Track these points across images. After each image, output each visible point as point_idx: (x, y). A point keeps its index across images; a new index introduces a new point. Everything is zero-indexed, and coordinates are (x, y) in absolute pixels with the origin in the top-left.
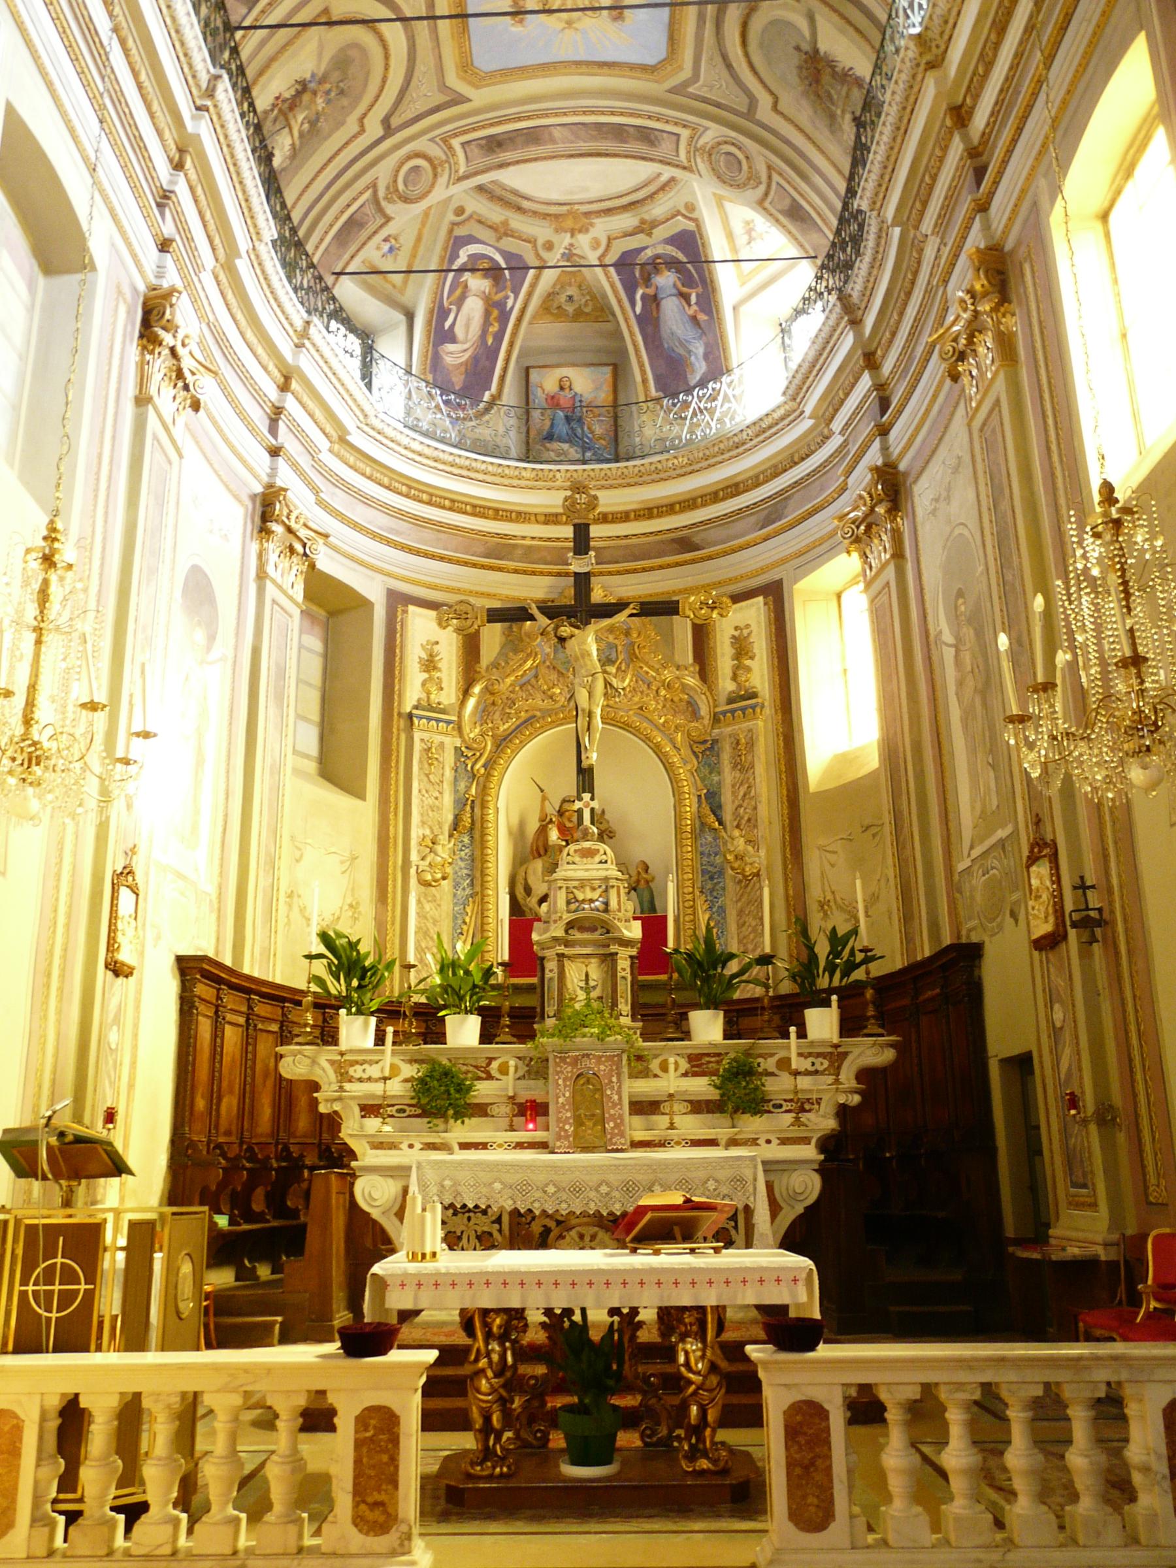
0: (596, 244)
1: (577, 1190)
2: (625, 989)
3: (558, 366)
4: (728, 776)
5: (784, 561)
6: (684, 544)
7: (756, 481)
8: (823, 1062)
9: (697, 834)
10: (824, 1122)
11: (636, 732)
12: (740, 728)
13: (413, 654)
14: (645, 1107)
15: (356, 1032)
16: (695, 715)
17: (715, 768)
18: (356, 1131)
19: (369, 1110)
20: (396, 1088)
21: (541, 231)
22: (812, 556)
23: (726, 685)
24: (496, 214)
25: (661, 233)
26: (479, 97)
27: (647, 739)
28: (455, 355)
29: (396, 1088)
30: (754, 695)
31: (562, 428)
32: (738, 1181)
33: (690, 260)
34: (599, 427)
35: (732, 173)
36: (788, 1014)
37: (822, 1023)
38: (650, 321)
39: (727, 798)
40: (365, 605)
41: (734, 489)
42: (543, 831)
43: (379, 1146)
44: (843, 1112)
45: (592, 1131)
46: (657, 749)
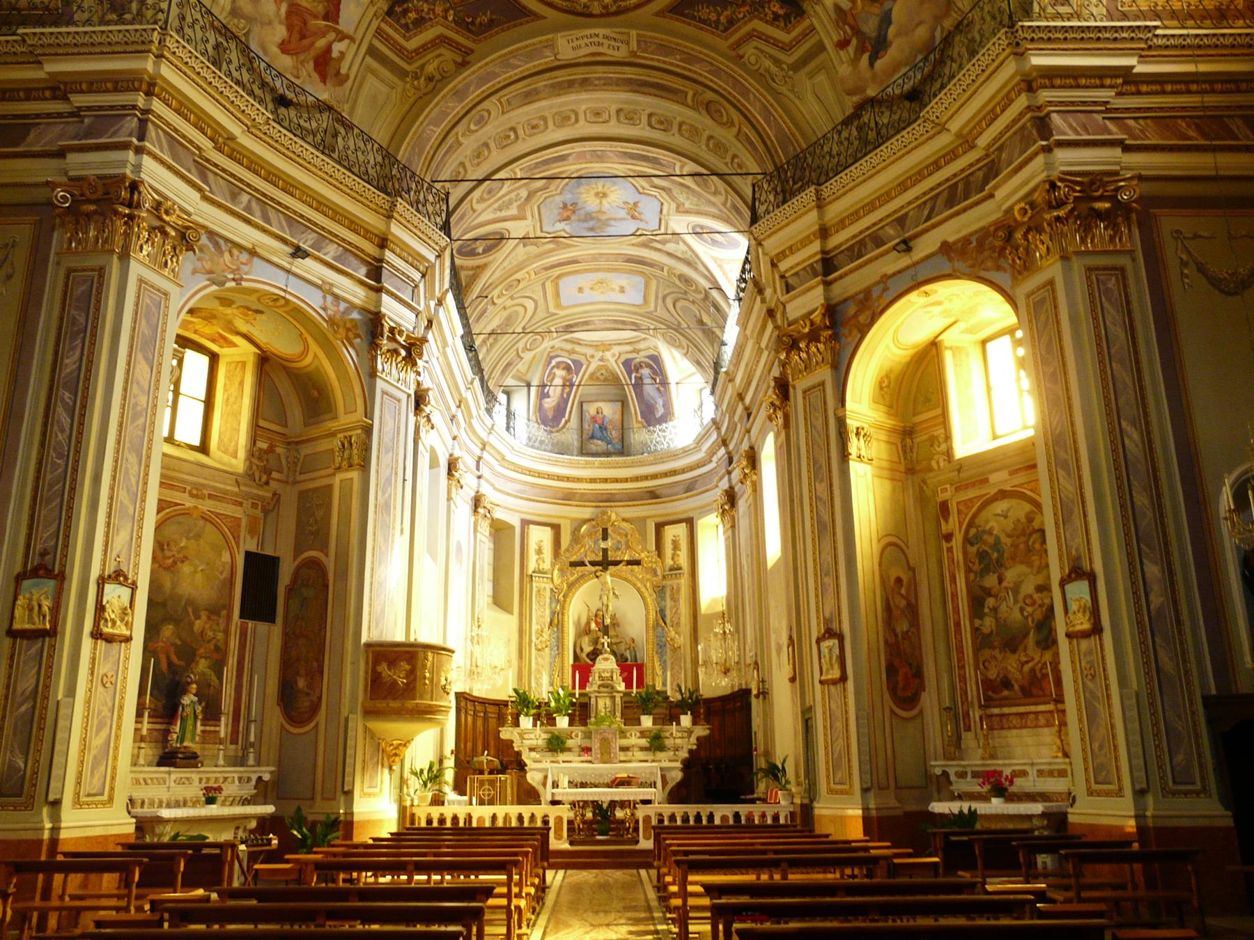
0: (614, 355)
1: (601, 776)
2: (619, 708)
3: (596, 401)
4: (669, 603)
5: (694, 509)
6: (653, 495)
7: (683, 471)
8: (686, 733)
9: (654, 628)
10: (684, 754)
11: (629, 582)
12: (674, 582)
13: (532, 547)
14: (624, 749)
15: (526, 722)
16: (655, 574)
17: (663, 599)
18: (526, 757)
19: (532, 749)
20: (540, 742)
21: (589, 351)
22: (705, 510)
23: (669, 562)
24: (569, 346)
25: (642, 354)
26: (562, 313)
27: (634, 585)
28: (549, 403)
29: (540, 742)
30: (680, 568)
31: (598, 434)
32: (652, 773)
33: (655, 364)
34: (615, 434)
35: (672, 342)
36: (673, 718)
37: (686, 720)
38: (638, 386)
39: (668, 613)
40: (512, 528)
41: (674, 473)
42: (588, 623)
43: (536, 761)
44: (690, 751)
45: (606, 757)
46: (638, 590)
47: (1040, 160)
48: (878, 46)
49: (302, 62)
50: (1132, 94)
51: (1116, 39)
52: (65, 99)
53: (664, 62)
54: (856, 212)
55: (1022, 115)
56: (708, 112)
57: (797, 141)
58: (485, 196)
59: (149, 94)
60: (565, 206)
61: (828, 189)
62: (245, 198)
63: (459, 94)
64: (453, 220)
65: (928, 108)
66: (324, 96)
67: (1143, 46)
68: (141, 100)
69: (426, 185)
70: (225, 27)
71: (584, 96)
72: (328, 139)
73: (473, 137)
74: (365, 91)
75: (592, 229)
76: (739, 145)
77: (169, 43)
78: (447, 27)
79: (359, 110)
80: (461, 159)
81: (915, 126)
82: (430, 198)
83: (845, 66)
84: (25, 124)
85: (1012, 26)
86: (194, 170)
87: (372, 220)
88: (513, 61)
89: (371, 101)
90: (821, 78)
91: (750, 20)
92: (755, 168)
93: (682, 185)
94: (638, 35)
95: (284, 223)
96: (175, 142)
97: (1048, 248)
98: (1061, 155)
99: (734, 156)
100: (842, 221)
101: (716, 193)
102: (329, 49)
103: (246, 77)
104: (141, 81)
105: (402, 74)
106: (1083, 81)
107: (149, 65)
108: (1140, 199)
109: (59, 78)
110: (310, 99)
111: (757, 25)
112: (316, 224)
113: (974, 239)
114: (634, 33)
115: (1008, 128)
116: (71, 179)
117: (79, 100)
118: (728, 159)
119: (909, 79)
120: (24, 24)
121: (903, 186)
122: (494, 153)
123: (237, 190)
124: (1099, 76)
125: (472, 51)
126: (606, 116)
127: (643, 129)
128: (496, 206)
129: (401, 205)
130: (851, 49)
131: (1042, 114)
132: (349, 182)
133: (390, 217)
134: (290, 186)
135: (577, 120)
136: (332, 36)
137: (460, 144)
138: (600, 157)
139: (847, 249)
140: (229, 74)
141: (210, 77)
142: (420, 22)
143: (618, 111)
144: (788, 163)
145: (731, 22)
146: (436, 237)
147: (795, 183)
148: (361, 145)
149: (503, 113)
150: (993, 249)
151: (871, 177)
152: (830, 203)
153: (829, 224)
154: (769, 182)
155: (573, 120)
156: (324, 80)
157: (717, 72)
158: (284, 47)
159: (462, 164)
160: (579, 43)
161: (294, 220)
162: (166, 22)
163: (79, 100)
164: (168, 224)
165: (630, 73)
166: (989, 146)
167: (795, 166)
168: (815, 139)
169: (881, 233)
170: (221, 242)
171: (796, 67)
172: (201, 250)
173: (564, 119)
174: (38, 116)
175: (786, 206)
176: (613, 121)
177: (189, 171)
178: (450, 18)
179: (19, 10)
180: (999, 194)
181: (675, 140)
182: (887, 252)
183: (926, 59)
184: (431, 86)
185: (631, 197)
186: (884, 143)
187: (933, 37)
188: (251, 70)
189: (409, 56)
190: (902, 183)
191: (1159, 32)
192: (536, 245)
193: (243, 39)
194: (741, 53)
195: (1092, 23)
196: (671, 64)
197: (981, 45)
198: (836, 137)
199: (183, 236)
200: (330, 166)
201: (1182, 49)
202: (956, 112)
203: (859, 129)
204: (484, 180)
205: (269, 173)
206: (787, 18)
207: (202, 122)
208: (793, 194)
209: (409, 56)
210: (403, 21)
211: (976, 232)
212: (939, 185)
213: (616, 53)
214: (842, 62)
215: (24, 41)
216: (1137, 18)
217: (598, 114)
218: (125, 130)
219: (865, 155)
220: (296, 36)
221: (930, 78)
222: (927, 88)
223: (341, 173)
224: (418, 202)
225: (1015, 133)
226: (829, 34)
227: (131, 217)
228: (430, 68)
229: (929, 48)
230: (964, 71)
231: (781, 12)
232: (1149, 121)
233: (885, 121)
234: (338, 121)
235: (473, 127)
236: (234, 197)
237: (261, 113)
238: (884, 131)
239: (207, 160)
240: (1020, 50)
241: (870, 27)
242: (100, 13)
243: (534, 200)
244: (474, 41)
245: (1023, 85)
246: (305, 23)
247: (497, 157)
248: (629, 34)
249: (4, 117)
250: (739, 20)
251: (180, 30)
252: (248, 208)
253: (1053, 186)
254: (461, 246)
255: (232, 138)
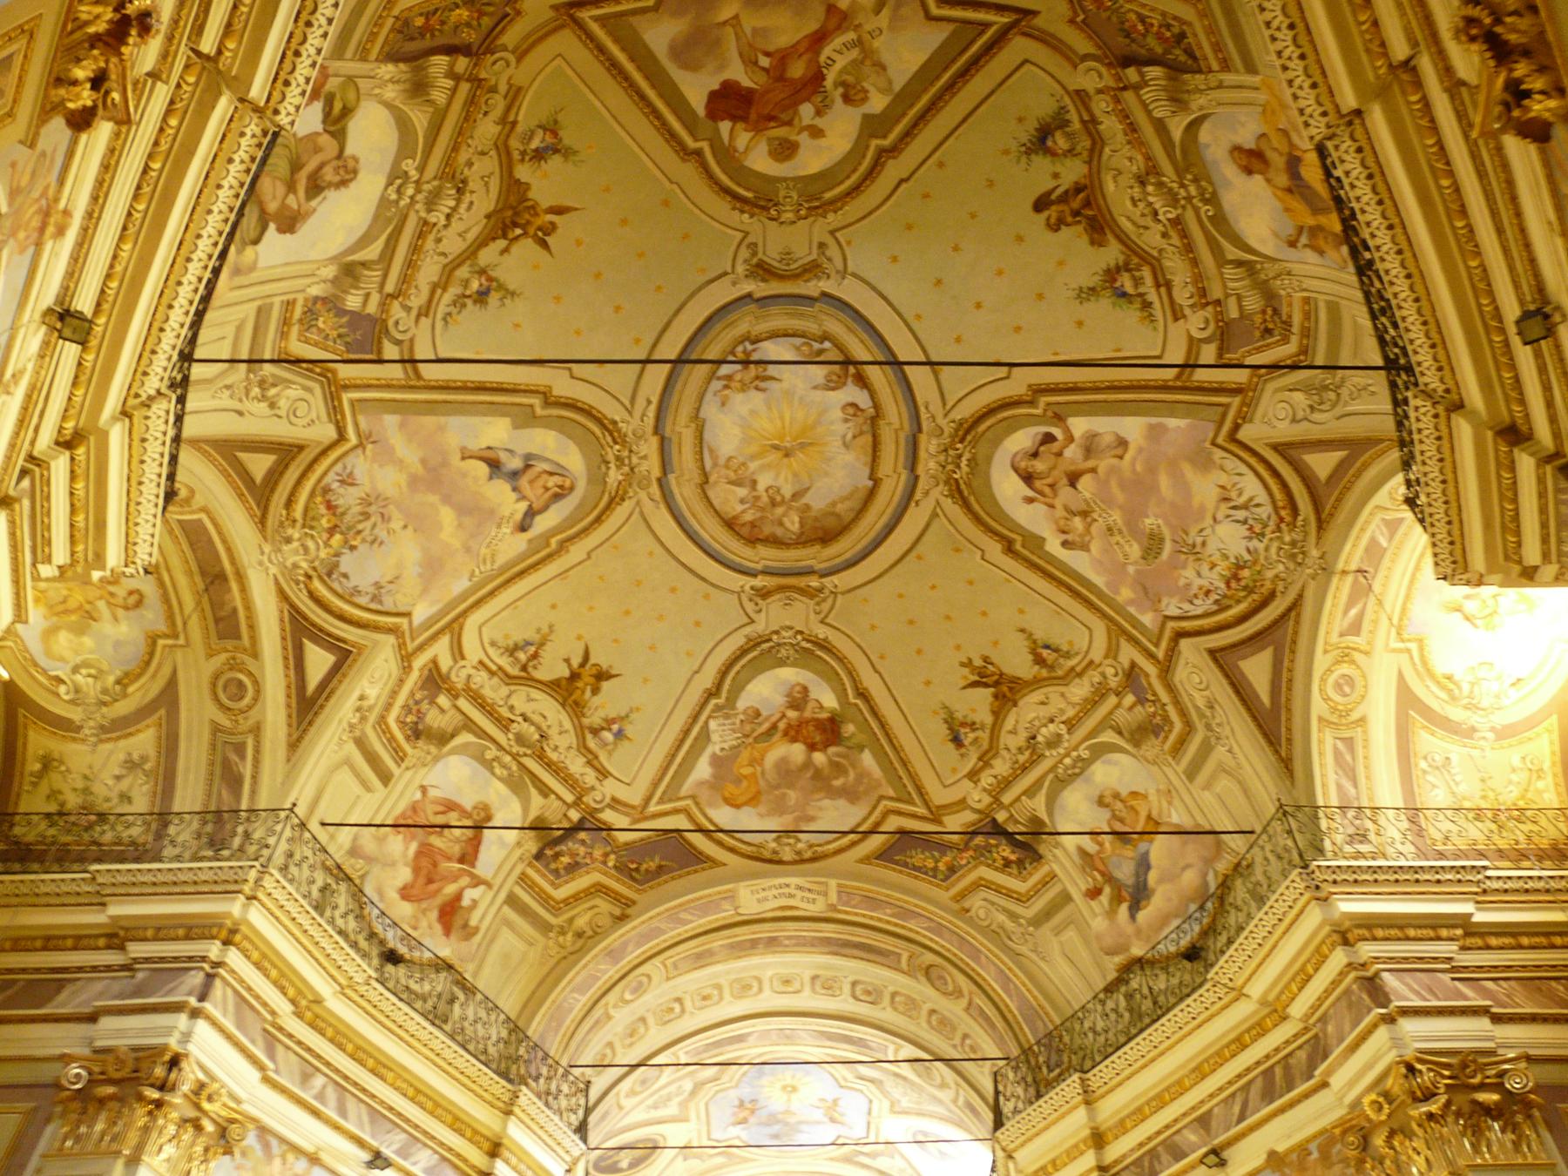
47: (1382, 1032)
48: (1138, 896)
49: (424, 912)
50: (1480, 948)
51: (1439, 881)
52: (122, 948)
53: (872, 918)
54: (1139, 1110)
55: (1342, 974)
56: (929, 979)
57: (1047, 1014)
58: (638, 1089)
59: (226, 943)
60: (741, 1104)
61: (1097, 1077)
62: (319, 1081)
63: (614, 955)
64: (592, 1119)
65: (1216, 969)
66: (445, 952)
67: (1475, 889)
68: (214, 950)
69: (561, 1071)
70: (339, 867)
71: (770, 959)
72: (442, 1007)
73: (626, 1010)
74: (496, 948)
75: (776, 1136)
76: (972, 1022)
77: (268, 882)
78: (605, 874)
79: (487, 971)
80: (609, 1038)
81: (1201, 991)
82: (565, 1088)
83: (1099, 918)
84: (59, 980)
85: (1306, 867)
86: (260, 1041)
87: (484, 1116)
88: (684, 916)
89: (502, 959)
90: (1070, 934)
91: (975, 867)
92: (992, 1050)
93: (897, 1075)
94: (839, 885)
95: (365, 1118)
96: (245, 1003)
97: (1427, 1160)
98: (1408, 1026)
99: (965, 1036)
100: (1122, 1122)
101: (943, 1085)
102: (458, 897)
103: (352, 924)
104: (221, 926)
105: (545, 928)
106: (1412, 932)
107: (235, 907)
108: (1537, 1089)
109: (122, 923)
110: (427, 955)
111: (984, 872)
112: (407, 1121)
113: (1313, 1147)
114: (833, 883)
115: (1327, 992)
116: (96, 1051)
117: (137, 950)
118: (957, 1041)
119: (1185, 933)
120: (99, 860)
121: (1200, 1072)
122: (653, 1030)
123: (310, 1070)
124: (1433, 926)
125: (634, 903)
126: (797, 986)
127: (845, 1000)
128: (650, 1102)
129: (526, 1096)
130: (1104, 898)
131: (1369, 974)
132: (460, 1063)
133: (508, 1113)
134: (381, 1066)
135: (760, 990)
136: (465, 881)
137: (609, 1018)
138: (788, 1037)
139: (1133, 1163)
140: (332, 922)
141: (306, 923)
142: (573, 868)
143: (814, 978)
144: (1038, 1043)
145: (952, 870)
146: (567, 1143)
147: (1050, 1070)
148: (482, 1014)
149: (668, 979)
150: (1345, 1161)
151: (1153, 1060)
152: (1103, 1096)
153: (1103, 1128)
154: (1016, 1069)
155: (755, 989)
156: (447, 931)
157: (939, 929)
158: (406, 893)
159: (610, 1045)
160: (763, 894)
161: (380, 1115)
162: (269, 859)
163: (137, 950)
164: (205, 1113)
165: (829, 930)
166: (1307, 1017)
167: (1048, 1047)
168: (1071, 1012)
169: (1177, 1138)
170: (274, 1142)
171: (1037, 922)
172: (244, 1154)
173: (744, 988)
174: (80, 969)
175: (1041, 1102)
176: (807, 991)
177: (253, 1042)
178: (611, 864)
179: (100, 845)
180: (1337, 1081)
181: (886, 1015)
182: (1192, 1167)
183: (1202, 908)
184: (580, 943)
185: (831, 1092)
186: (1163, 1015)
187: (1206, 884)
188: (360, 917)
189: (555, 907)
190: (1197, 1069)
191: (1489, 873)
192: (698, 1157)
193: (357, 881)
194: (966, 904)
195: (1403, 863)
196: (880, 920)
197: (1271, 888)
198: (1077, 1027)
199: (223, 1133)
200: (439, 1040)
201: (1526, 894)
202: (1254, 973)
203: (1129, 997)
204: (638, 1065)
205: (358, 1048)
206: (1020, 863)
207: (284, 978)
208: (1050, 1085)
209: (555, 907)
210: (553, 866)
211: (1315, 1137)
212: (1248, 1070)
213: (811, 907)
214: (1095, 915)
215: (94, 879)
216: (1457, 857)
217: (787, 982)
218: (185, 988)
219: (1141, 1031)
220: (422, 880)
221: (1210, 931)
222: (1210, 943)
223: (452, 1050)
224: (548, 1094)
225: (1338, 999)
226: (1077, 884)
227: (159, 1104)
228: (581, 922)
229: (1203, 898)
230: (1255, 921)
231: (1013, 857)
232: (1513, 983)
233: (1163, 986)
234: (457, 983)
235: (628, 996)
236: (305, 1078)
237: (361, 969)
238: (1161, 999)
239: (281, 1029)
240: (1322, 894)
241: (1125, 872)
242: (194, 849)
243: (702, 1093)
244: (638, 891)
245: (1336, 937)
246: (435, 865)
247: (656, 1036)
248: (826, 884)
249: (19, 943)
250: (962, 867)
251: (284, 869)
252: (320, 1097)
253: (1411, 1069)
254: (601, 1159)
255: (318, 1001)
